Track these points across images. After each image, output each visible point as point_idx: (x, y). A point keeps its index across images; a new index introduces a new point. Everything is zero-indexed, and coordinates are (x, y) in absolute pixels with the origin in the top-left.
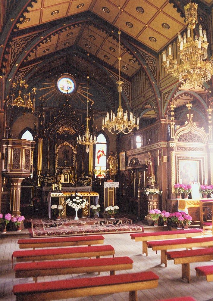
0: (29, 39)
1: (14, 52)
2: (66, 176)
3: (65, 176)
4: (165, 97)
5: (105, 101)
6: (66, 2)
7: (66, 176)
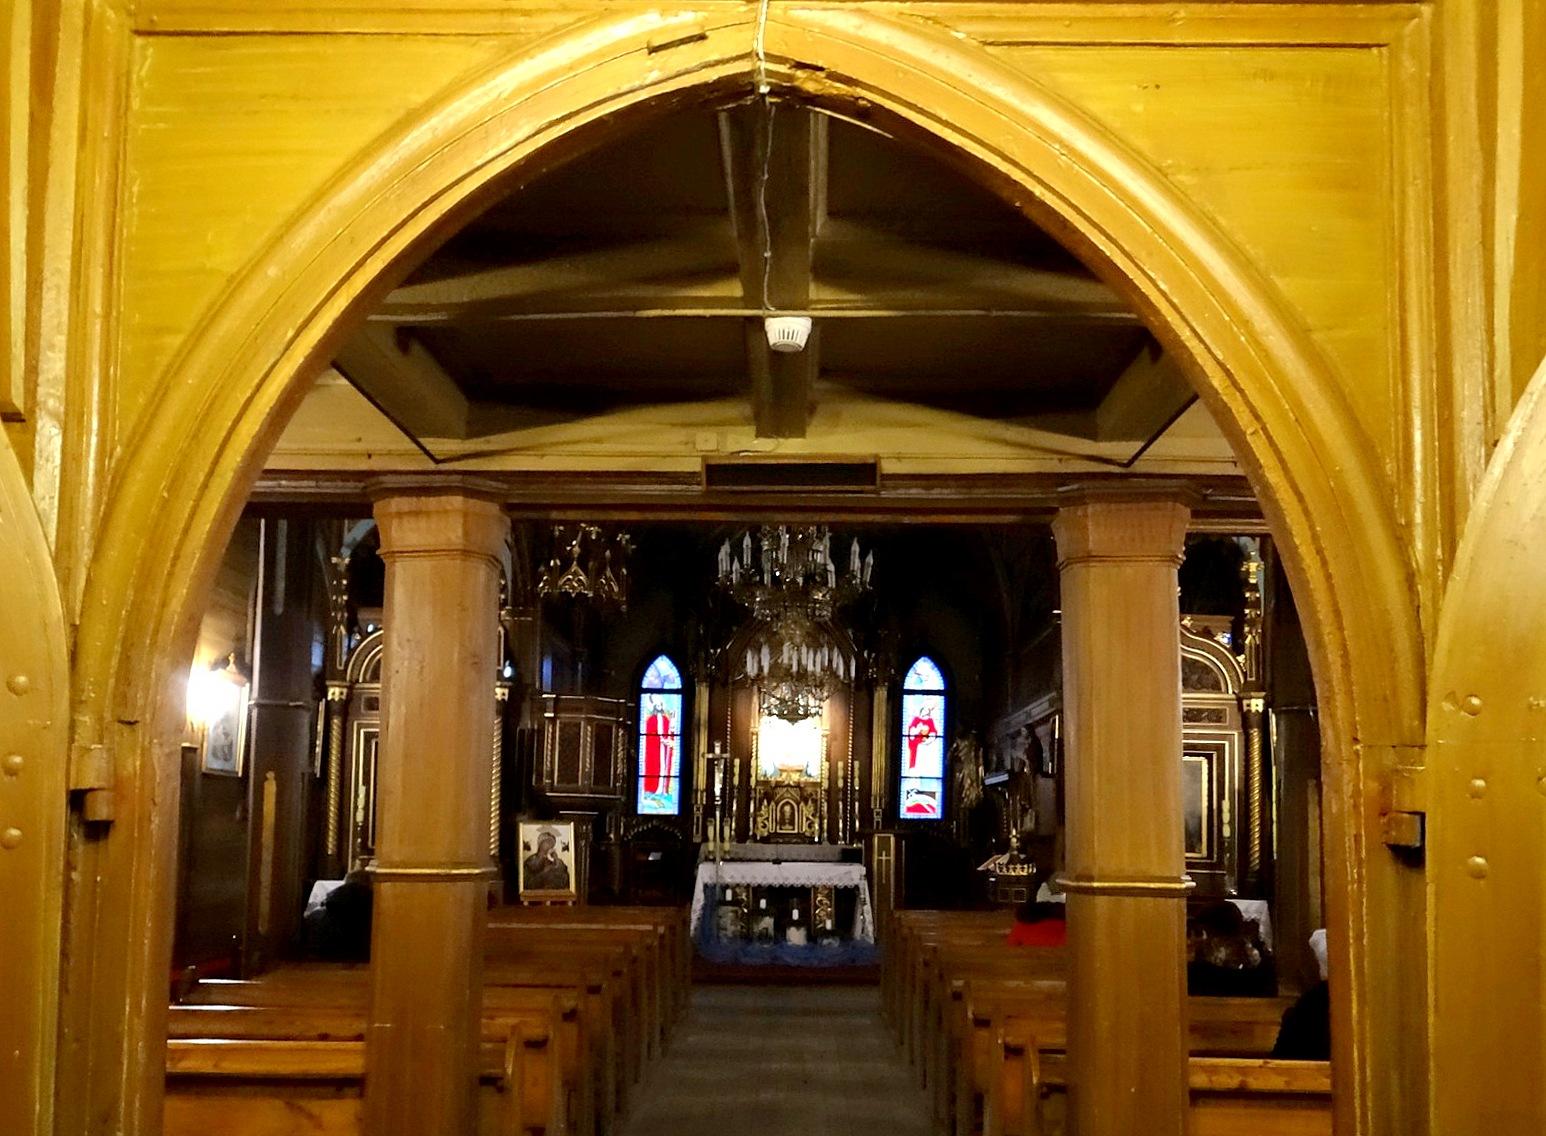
2: (787, 809)
7: (787, 809)
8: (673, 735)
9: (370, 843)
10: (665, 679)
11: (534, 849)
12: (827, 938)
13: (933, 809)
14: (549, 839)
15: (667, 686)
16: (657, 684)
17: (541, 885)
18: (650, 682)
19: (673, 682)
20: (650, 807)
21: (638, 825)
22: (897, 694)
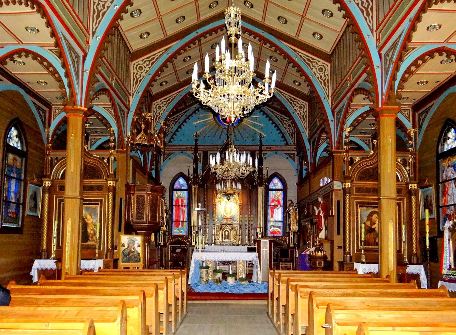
0: (153, 59)
1: (136, 77)
2: (227, 233)
3: (225, 233)
4: (420, 119)
5: (174, 134)
6: (73, 4)
7: (227, 233)
8: (185, 206)
9: (60, 244)
10: (182, 185)
11: (126, 246)
12: (243, 281)
13: (280, 233)
14: (133, 242)
15: (183, 188)
16: (179, 187)
17: (129, 261)
18: (177, 186)
19: (185, 186)
20: (176, 233)
21: (172, 239)
22: (267, 190)
